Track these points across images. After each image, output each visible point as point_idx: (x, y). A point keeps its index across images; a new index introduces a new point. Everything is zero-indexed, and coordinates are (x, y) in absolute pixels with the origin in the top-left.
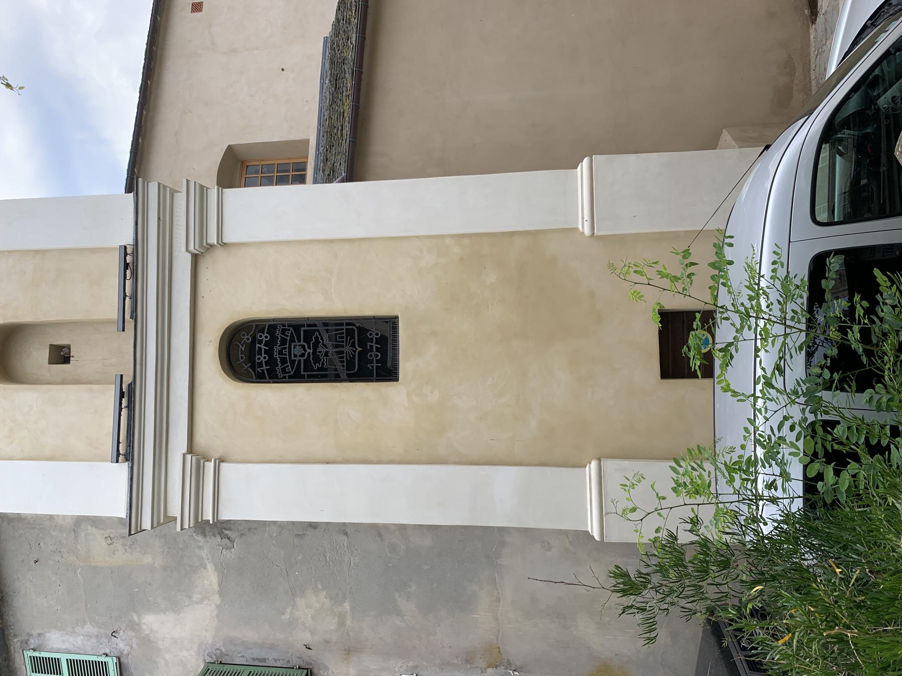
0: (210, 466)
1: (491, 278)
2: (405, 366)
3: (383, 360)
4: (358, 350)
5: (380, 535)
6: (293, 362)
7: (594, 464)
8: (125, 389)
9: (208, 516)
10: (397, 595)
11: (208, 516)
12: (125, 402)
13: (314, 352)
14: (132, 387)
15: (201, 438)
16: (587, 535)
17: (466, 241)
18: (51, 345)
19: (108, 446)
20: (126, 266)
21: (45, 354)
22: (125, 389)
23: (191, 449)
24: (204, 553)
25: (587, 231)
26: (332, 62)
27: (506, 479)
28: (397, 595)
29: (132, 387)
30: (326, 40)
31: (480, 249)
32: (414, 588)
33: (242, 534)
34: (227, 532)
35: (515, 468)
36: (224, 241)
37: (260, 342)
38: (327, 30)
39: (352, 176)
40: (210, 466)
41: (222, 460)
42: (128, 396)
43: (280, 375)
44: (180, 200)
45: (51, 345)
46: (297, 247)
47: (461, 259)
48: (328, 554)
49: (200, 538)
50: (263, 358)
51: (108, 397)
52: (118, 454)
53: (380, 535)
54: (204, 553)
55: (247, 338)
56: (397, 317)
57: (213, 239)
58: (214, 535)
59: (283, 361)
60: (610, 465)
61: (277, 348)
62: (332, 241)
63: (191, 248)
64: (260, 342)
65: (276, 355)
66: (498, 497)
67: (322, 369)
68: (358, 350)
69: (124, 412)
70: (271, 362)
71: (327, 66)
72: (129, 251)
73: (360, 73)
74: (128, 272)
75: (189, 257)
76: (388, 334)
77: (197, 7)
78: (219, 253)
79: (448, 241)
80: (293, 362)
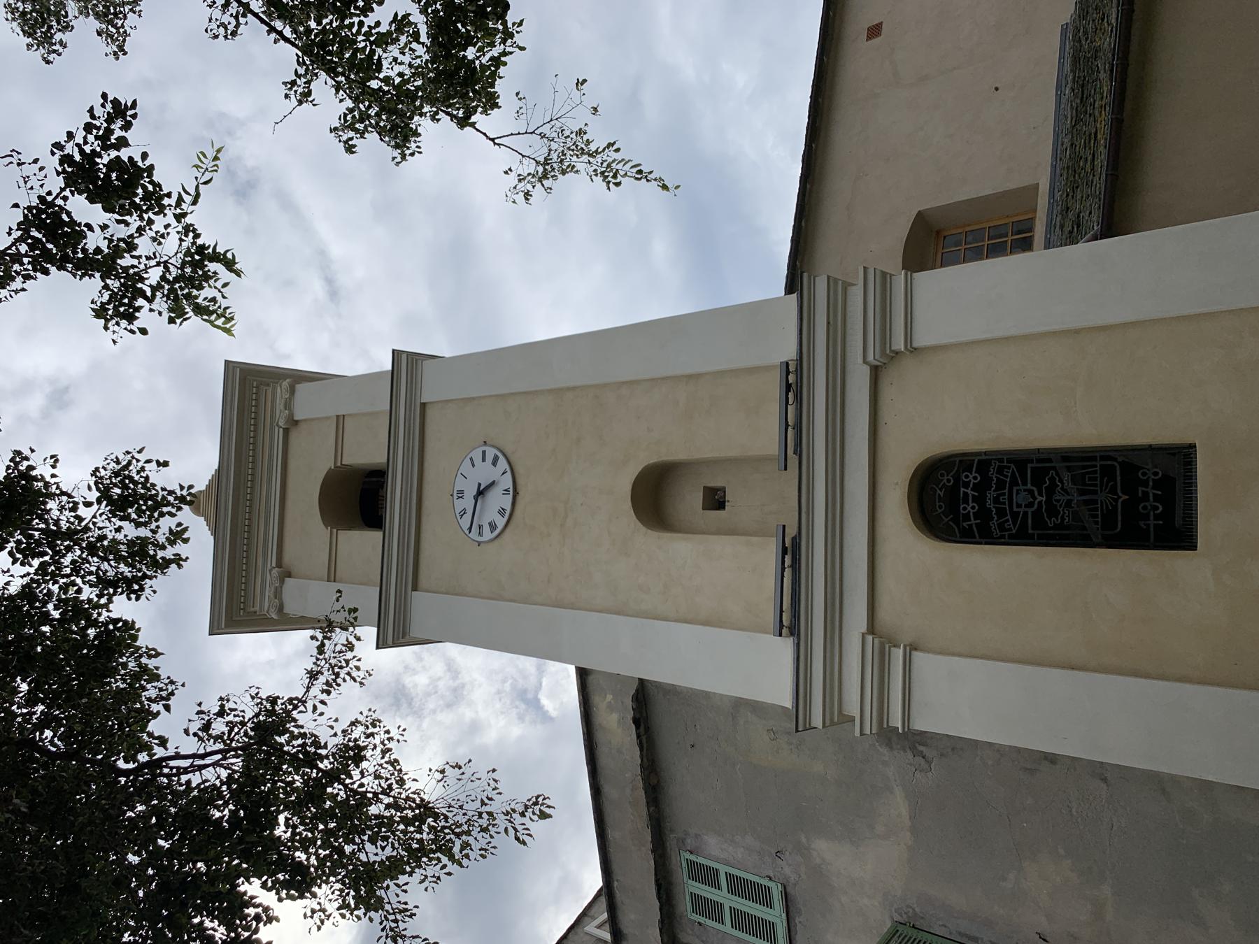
0: (898, 654)
2: (1210, 521)
6: (1015, 516)
13: (1049, 501)
21: (699, 496)
23: (872, 628)
26: (1075, 60)
30: (1064, 29)
37: (966, 485)
40: (898, 654)
42: (792, 552)
43: (996, 532)
44: (856, 294)
50: (971, 508)
52: (782, 626)
55: (947, 479)
57: (899, 344)
59: (1001, 513)
61: (991, 494)
62: (1077, 332)
63: (870, 358)
64: (966, 485)
65: (989, 504)
69: (788, 573)
70: (983, 514)
71: (1068, 68)
74: (791, 395)
75: (867, 369)
80: (1015, 516)
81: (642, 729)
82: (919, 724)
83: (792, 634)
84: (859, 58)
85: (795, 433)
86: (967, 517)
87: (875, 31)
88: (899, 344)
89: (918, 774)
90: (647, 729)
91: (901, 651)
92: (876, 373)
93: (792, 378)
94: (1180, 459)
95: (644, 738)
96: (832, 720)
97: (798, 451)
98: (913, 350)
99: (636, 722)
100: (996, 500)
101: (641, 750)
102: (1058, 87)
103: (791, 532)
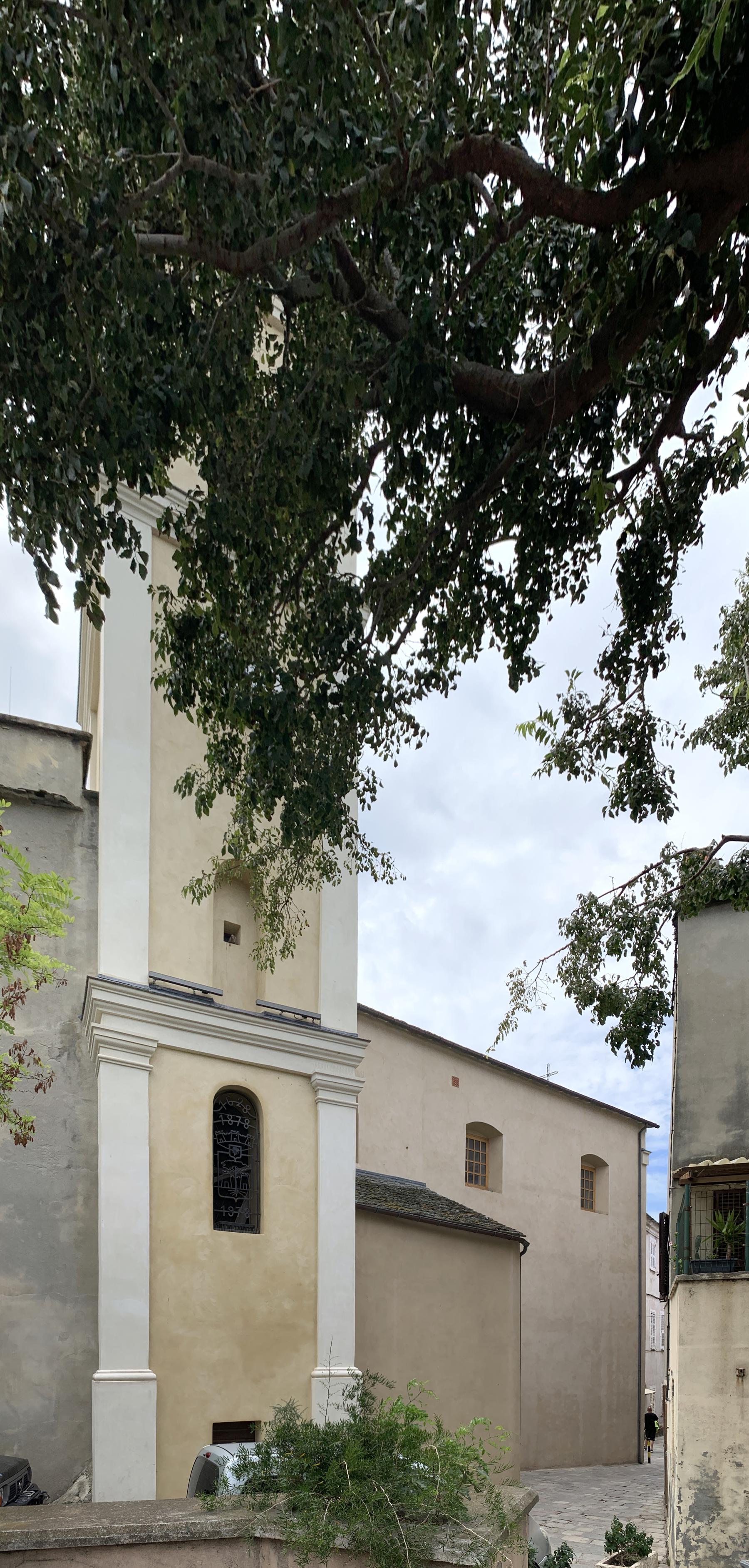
0: (145, 1062)
1: (287, 1305)
2: (226, 1237)
3: (227, 1218)
4: (236, 1199)
5: (69, 1197)
6: (226, 1144)
7: (153, 1375)
8: (210, 995)
9: (103, 1053)
10: (12, 1206)
11: (103, 1053)
12: (198, 993)
13: (234, 1164)
14: (210, 1002)
15: (168, 1057)
16: (96, 1367)
17: (313, 1289)
18: (239, 927)
19: (162, 970)
20: (305, 1017)
21: (233, 921)
22: (210, 995)
23: (160, 1046)
24: (43, 1027)
25: (316, 1373)
26: (413, 1191)
27: (140, 1308)
28: (12, 1206)
29: (210, 1002)
30: (424, 1185)
31: (307, 1298)
32: (19, 1222)
33: (64, 1069)
34: (66, 1055)
35: (146, 1314)
36: (320, 1105)
37: (243, 1120)
38: (432, 1187)
39: (361, 1210)
40: (145, 1062)
41: (150, 1073)
42: (203, 998)
43: (217, 1133)
44: (349, 1073)
45: (239, 927)
46: (316, 1160)
47: (300, 1285)
48: (48, 1148)
49: (58, 1027)
50: (230, 1121)
51: (201, 978)
52: (156, 979)
53: (69, 1197)
54: (43, 1027)
55: (246, 1109)
56: (258, 1232)
57: (322, 1095)
58: (62, 1042)
59: (228, 1137)
60: (153, 1386)
61: (237, 1133)
62: (316, 1189)
63: (317, 1077)
64: (243, 1120)
65: (232, 1132)
66: (123, 1301)
67: (221, 1166)
68: (236, 1199)
69: (191, 991)
70: (227, 1127)
71: (408, 1185)
72: (316, 1021)
73: (418, 1220)
74: (300, 1017)
75: (310, 1072)
76: (239, 1222)
77: (455, 1082)
78: (309, 1098)
79: (313, 1276)
80: (226, 1144)
81: (34, 797)
82: (103, 1068)
83: (151, 985)
84: (446, 1067)
85: (275, 1016)
86: (225, 1118)
87: (455, 1082)
88: (322, 1095)
89: (46, 1048)
90: (34, 802)
91: (147, 1064)
92: (308, 1077)
93: (309, 1020)
94: (252, 1225)
95: (26, 796)
96: (97, 1005)
97: (267, 1016)
98: (317, 1102)
99: (41, 794)
100: (234, 1136)
101: (15, 791)
102: (400, 1179)
103: (217, 999)
